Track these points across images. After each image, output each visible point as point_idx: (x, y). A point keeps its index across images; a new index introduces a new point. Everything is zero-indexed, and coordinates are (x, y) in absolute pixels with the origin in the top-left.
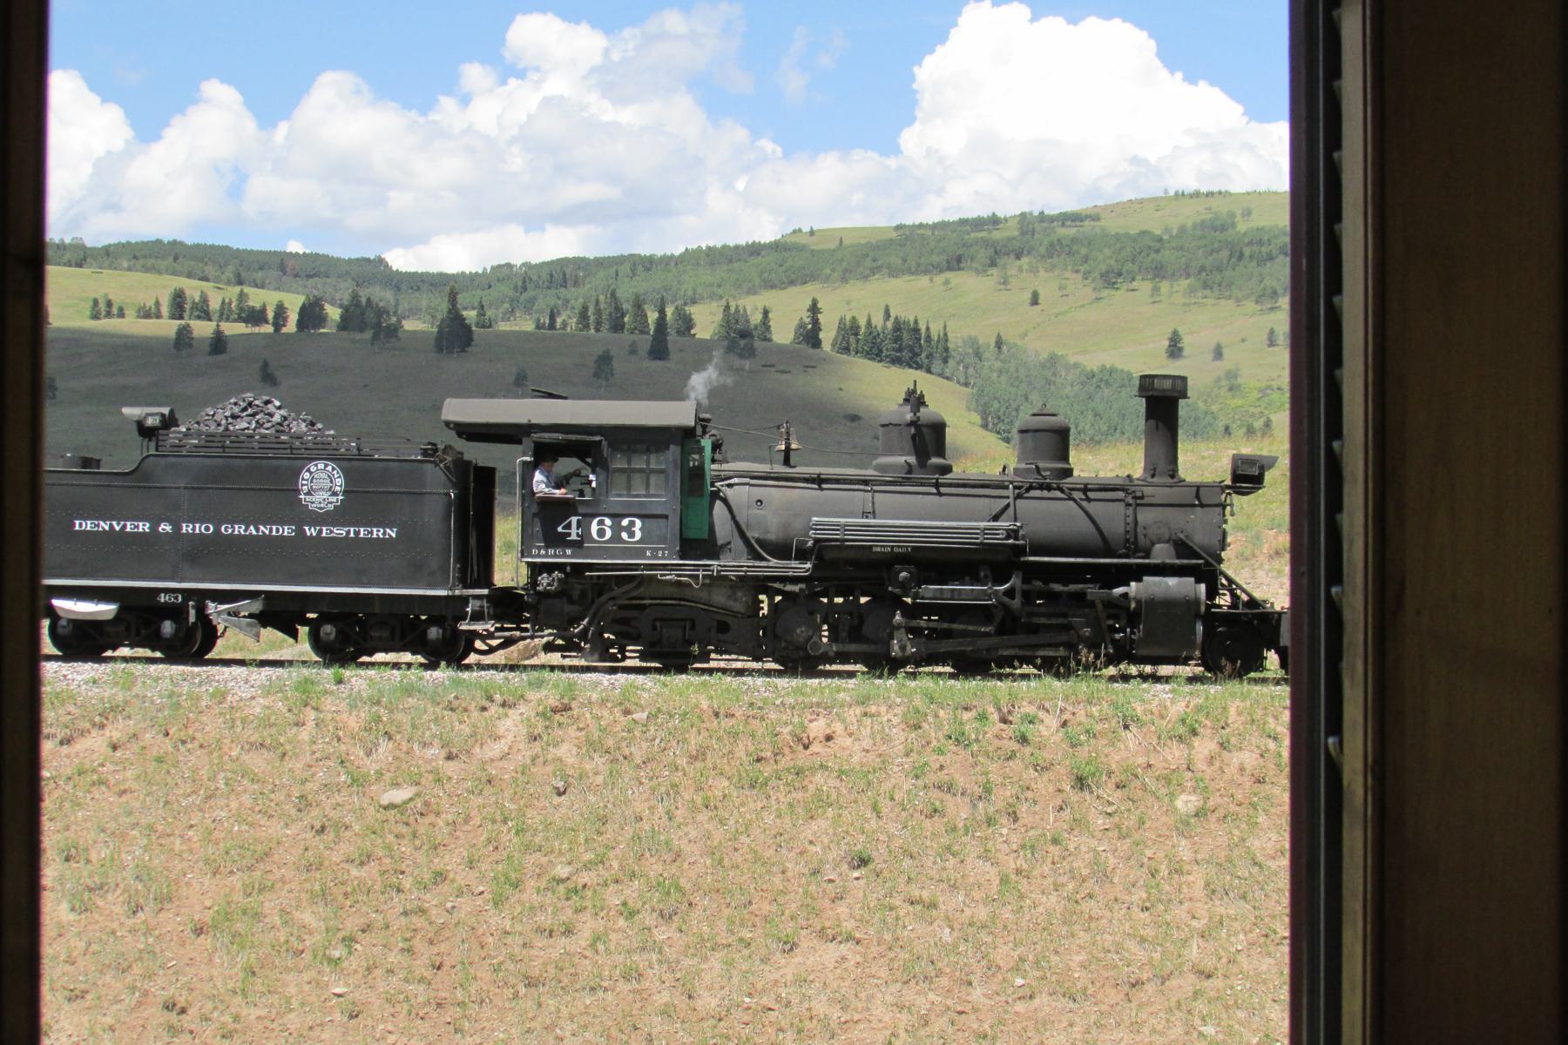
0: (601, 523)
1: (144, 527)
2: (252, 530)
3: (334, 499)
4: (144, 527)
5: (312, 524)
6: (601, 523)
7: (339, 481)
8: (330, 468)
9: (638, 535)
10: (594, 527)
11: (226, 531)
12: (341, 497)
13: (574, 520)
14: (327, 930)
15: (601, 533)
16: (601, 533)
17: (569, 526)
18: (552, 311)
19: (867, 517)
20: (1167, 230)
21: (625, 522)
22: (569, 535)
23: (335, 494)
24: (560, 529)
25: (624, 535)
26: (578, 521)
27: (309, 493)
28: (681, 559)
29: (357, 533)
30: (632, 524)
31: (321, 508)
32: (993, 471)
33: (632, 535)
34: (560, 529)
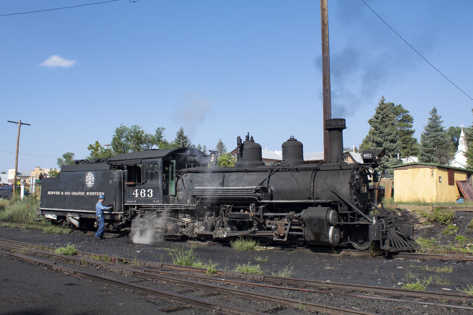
0: (143, 191)
1: (59, 193)
2: (62, 193)
3: (92, 184)
4: (59, 193)
5: (88, 191)
6: (143, 191)
7: (93, 178)
8: (91, 174)
9: (370, 156)
10: (141, 193)
11: (69, 193)
12: (94, 183)
13: (137, 190)
14: (387, 116)
15: (143, 195)
16: (143, 195)
17: (135, 193)
18: (241, 156)
19: (228, 279)
20: (402, 107)
21: (148, 191)
22: (135, 195)
23: (92, 182)
25: (148, 195)
26: (138, 191)
27: (87, 182)
28: (163, 204)
29: (96, 194)
30: (150, 191)
31: (90, 187)
32: (350, 158)
33: (150, 195)
34: (133, 194)
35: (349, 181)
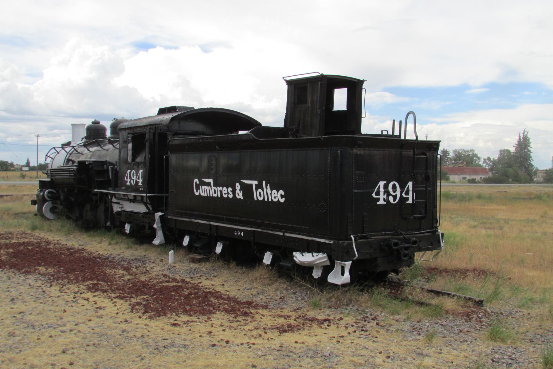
0: (395, 197)
6: (395, 197)
15: (394, 187)
16: (394, 187)
17: (378, 193)
22: (378, 200)
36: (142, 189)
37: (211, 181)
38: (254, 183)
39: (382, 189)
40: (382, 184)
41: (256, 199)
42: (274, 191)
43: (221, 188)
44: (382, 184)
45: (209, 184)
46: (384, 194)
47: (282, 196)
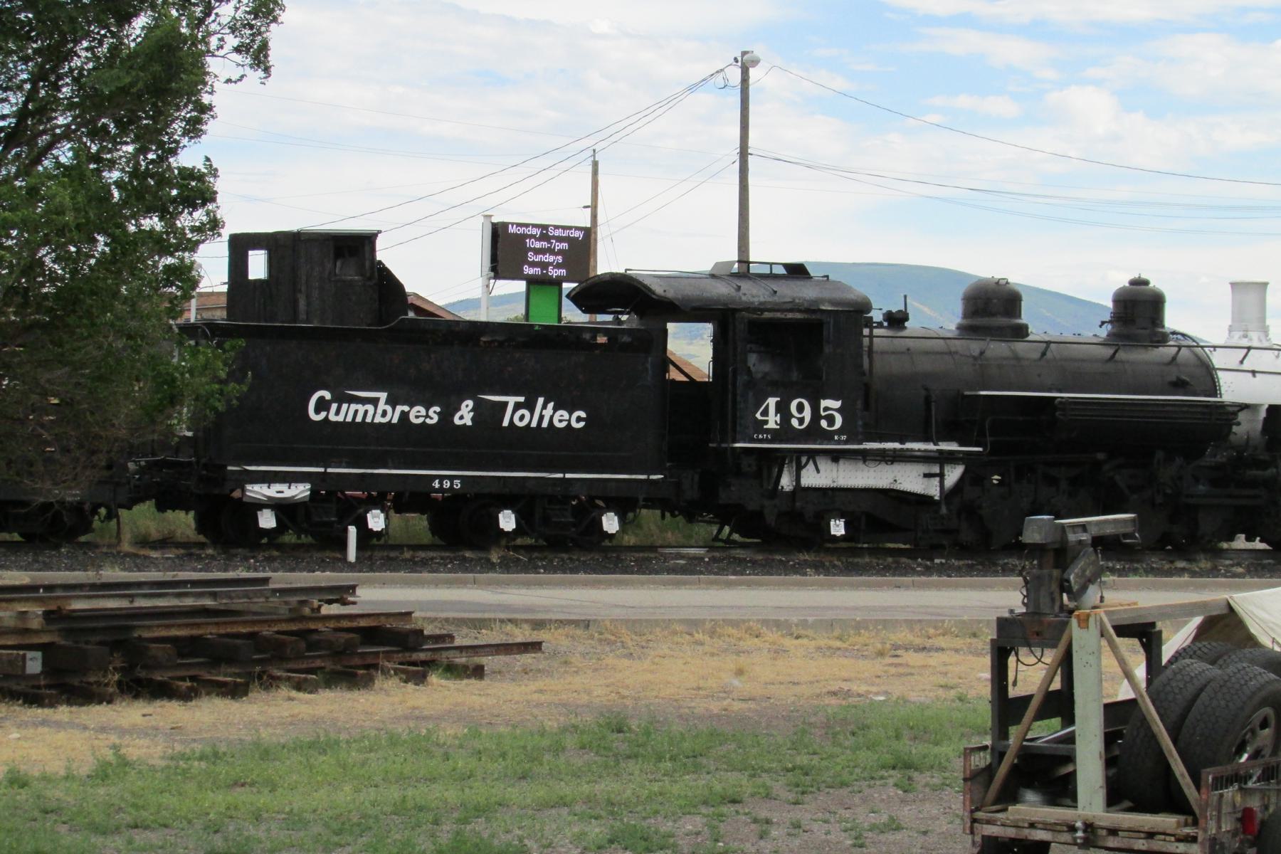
0: (801, 421)
6: (801, 421)
10: (449, 484)
15: (800, 408)
16: (800, 408)
17: (765, 413)
22: (766, 422)
24: (758, 416)
26: (777, 403)
35: (896, 320)
36: (844, 438)
37: (383, 396)
38: (512, 400)
39: (772, 410)
40: (772, 402)
41: (506, 423)
42: (563, 414)
43: (406, 408)
44: (772, 402)
45: (375, 402)
46: (776, 416)
47: (579, 419)
